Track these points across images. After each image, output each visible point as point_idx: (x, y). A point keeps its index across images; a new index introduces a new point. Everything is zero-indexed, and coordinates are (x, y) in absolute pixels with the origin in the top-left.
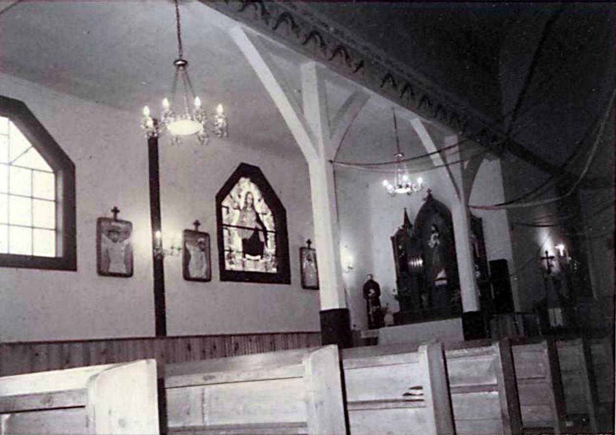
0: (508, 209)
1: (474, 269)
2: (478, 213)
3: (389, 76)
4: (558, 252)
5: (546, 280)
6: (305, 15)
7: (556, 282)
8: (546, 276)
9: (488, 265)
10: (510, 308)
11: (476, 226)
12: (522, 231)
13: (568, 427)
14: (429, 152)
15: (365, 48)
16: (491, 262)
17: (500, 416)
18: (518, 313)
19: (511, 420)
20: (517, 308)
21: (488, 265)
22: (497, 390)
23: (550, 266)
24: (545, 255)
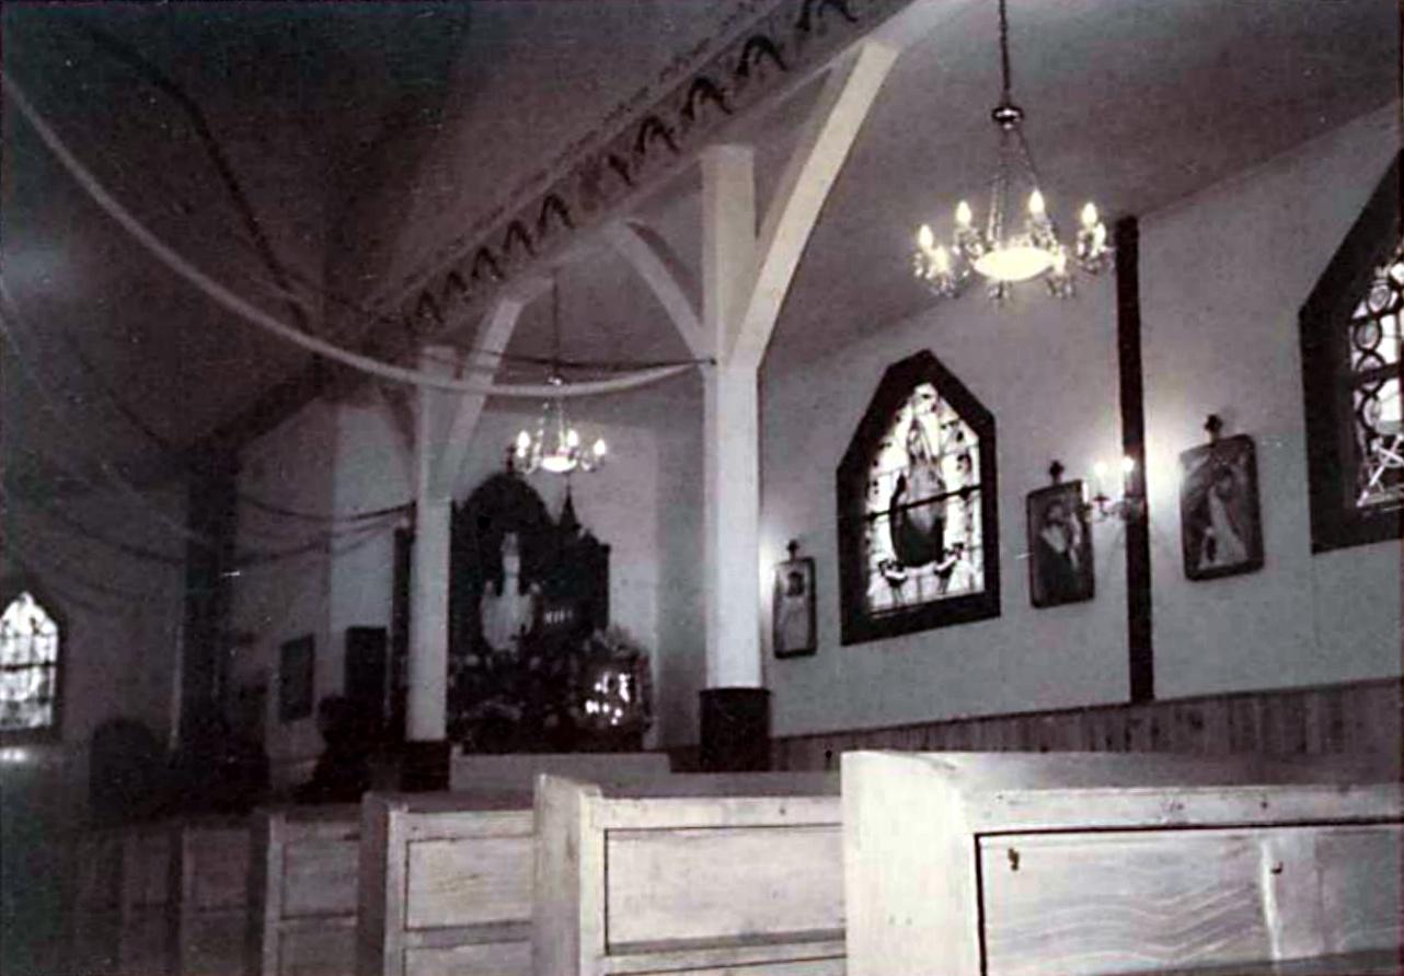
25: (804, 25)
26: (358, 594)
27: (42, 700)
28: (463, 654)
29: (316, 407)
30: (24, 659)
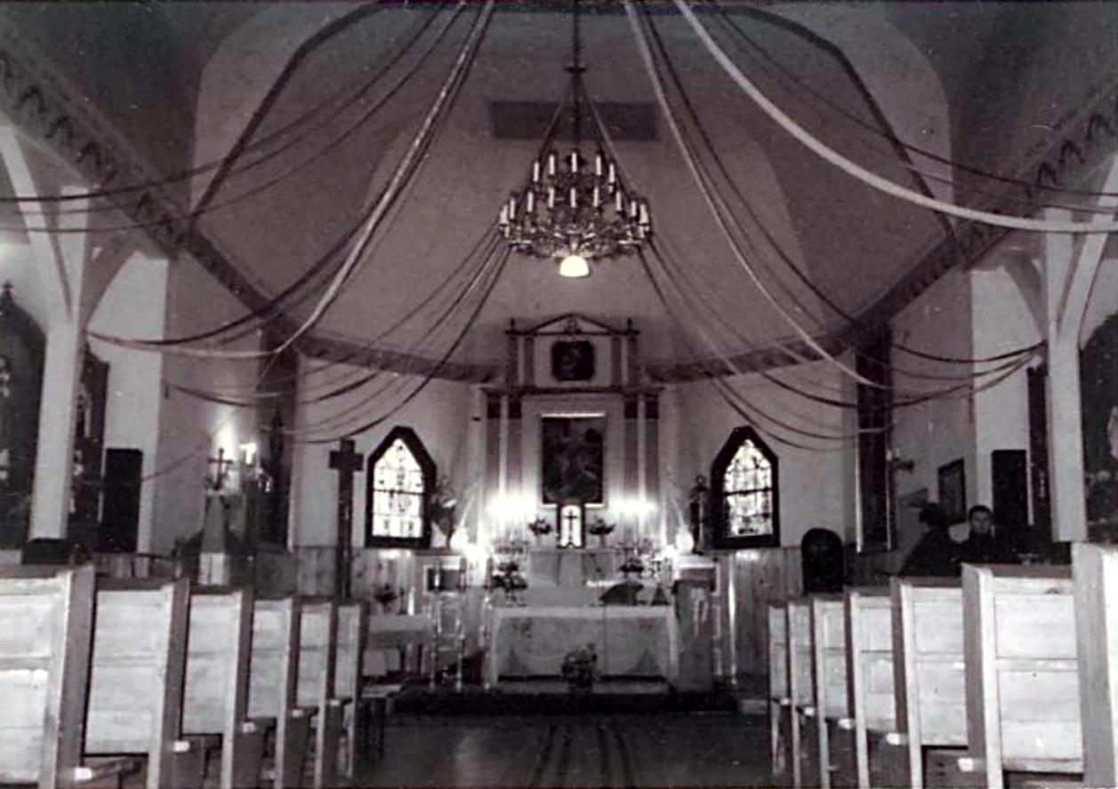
0: (166, 355)
1: (71, 458)
2: (103, 352)
3: (35, 91)
4: (244, 454)
5: (209, 500)
6: (335, 460)
7: (227, 504)
8: (211, 492)
9: (104, 455)
10: (130, 546)
11: (94, 375)
12: (185, 397)
13: (179, 754)
14: (19, 195)
15: (45, 75)
16: (110, 451)
17: (40, 723)
18: (142, 555)
19: (61, 729)
20: (143, 545)
21: (104, 455)
22: (45, 669)
23: (221, 476)
24: (217, 456)
25: (1089, 137)
26: (999, 423)
27: (765, 516)
28: (1096, 471)
29: (954, 275)
30: (751, 487)
